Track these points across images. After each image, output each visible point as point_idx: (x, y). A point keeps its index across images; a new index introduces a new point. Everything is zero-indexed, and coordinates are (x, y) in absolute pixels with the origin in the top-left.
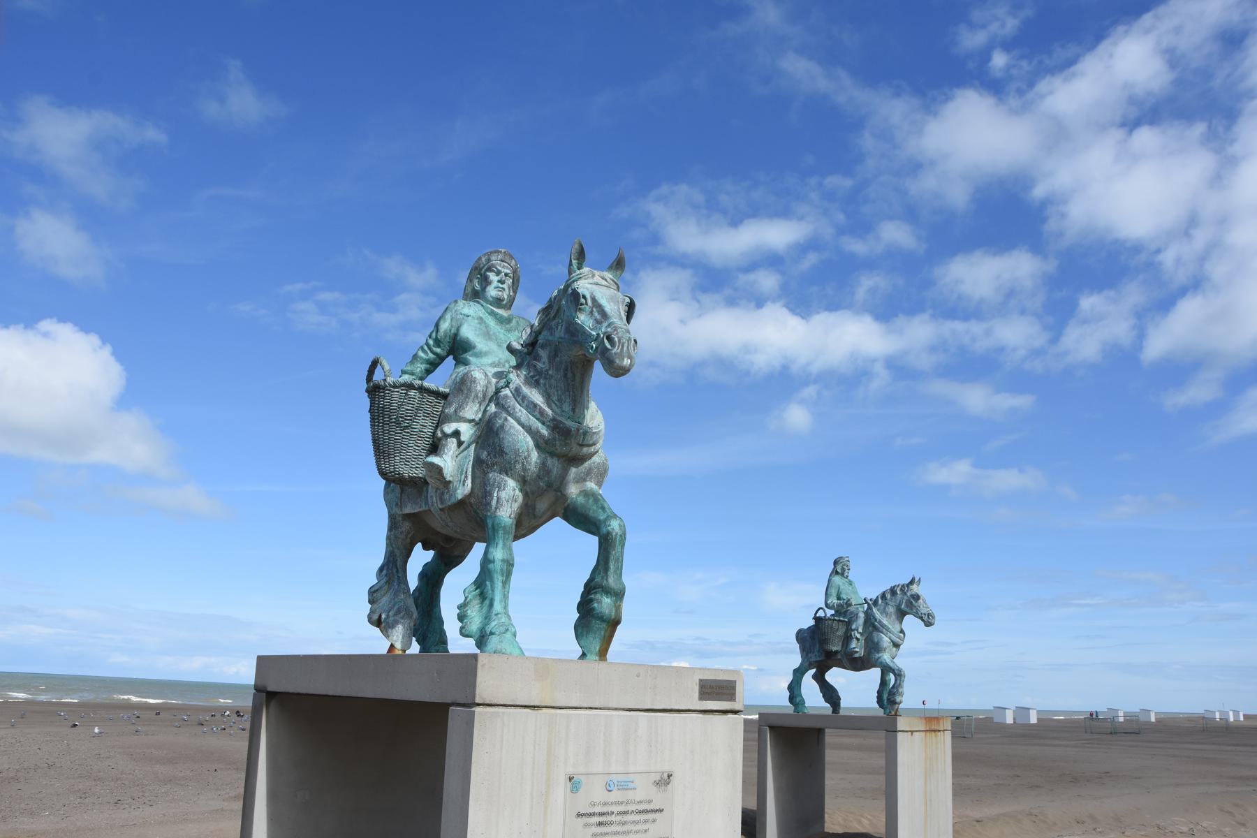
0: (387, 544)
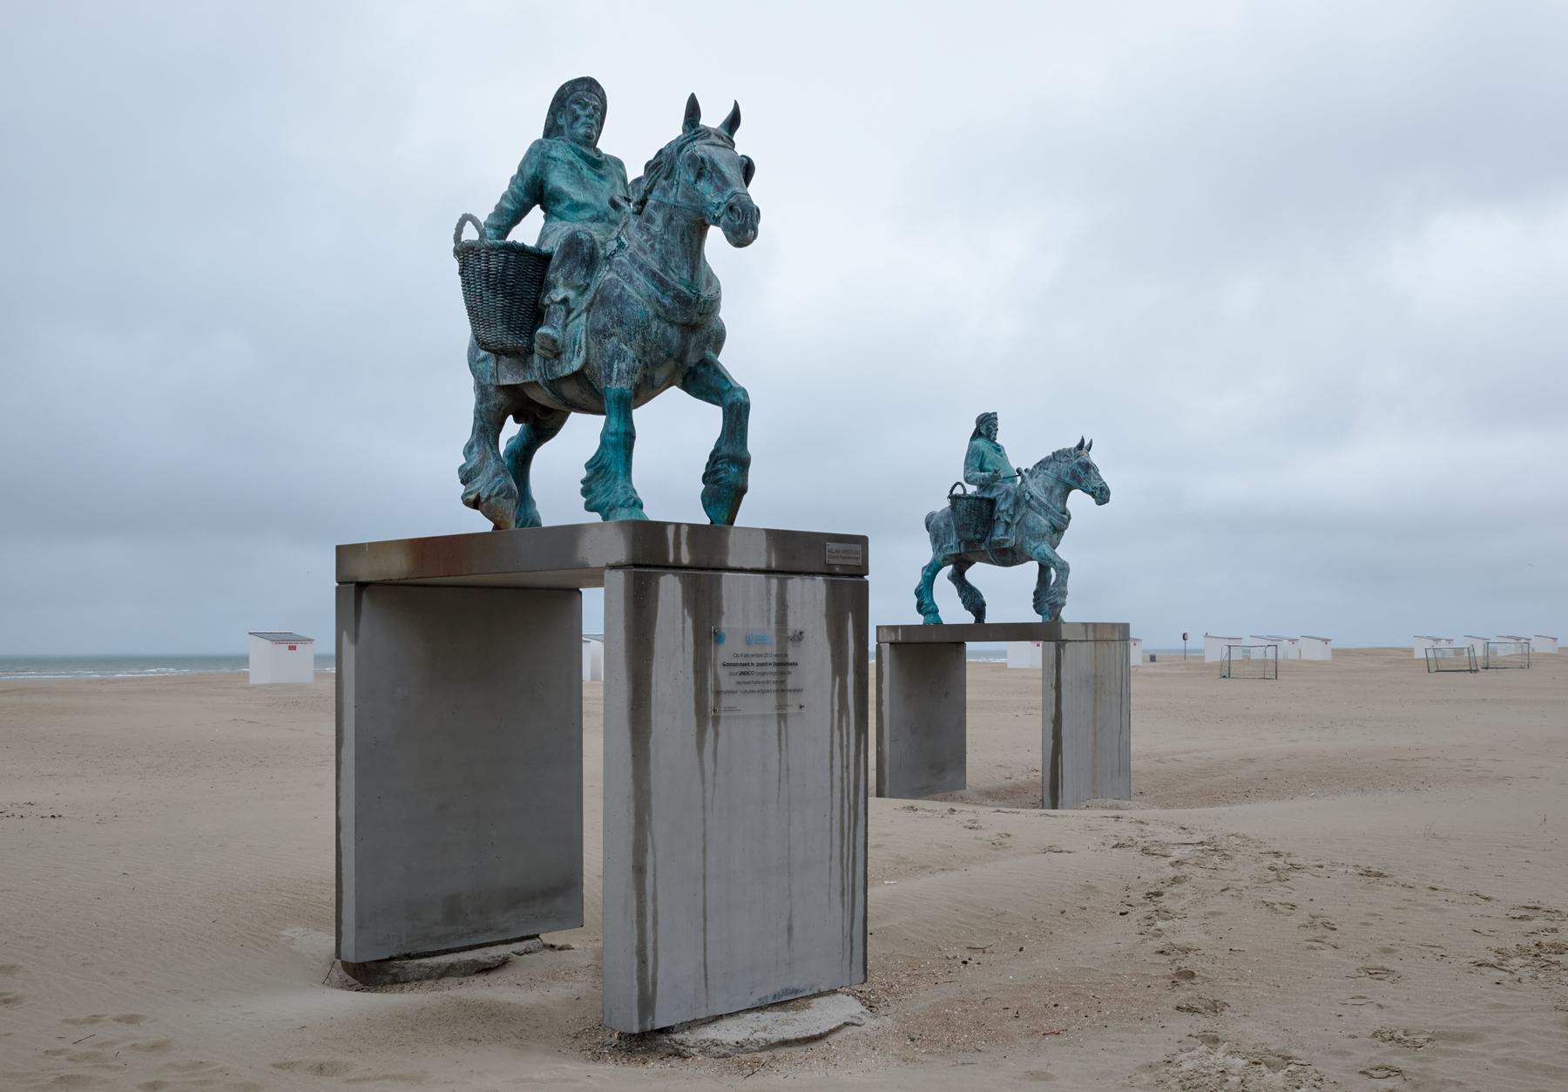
0: (475, 418)
